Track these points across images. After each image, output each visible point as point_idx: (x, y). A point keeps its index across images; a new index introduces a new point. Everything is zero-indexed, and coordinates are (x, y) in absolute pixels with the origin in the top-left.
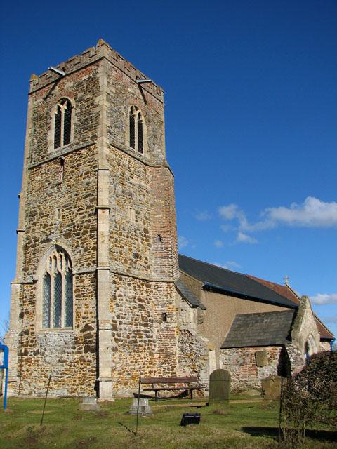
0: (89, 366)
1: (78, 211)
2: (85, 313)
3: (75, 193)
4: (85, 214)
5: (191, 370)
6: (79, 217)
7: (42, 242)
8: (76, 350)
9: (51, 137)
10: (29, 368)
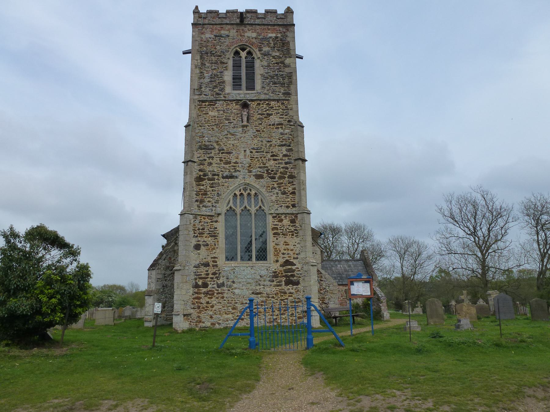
0: (290, 298)
1: (271, 156)
2: (285, 250)
3: (267, 139)
4: (281, 161)
5: (321, 302)
6: (272, 162)
7: (223, 177)
8: (275, 283)
9: (228, 76)
10: (210, 301)
